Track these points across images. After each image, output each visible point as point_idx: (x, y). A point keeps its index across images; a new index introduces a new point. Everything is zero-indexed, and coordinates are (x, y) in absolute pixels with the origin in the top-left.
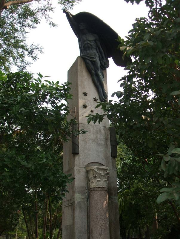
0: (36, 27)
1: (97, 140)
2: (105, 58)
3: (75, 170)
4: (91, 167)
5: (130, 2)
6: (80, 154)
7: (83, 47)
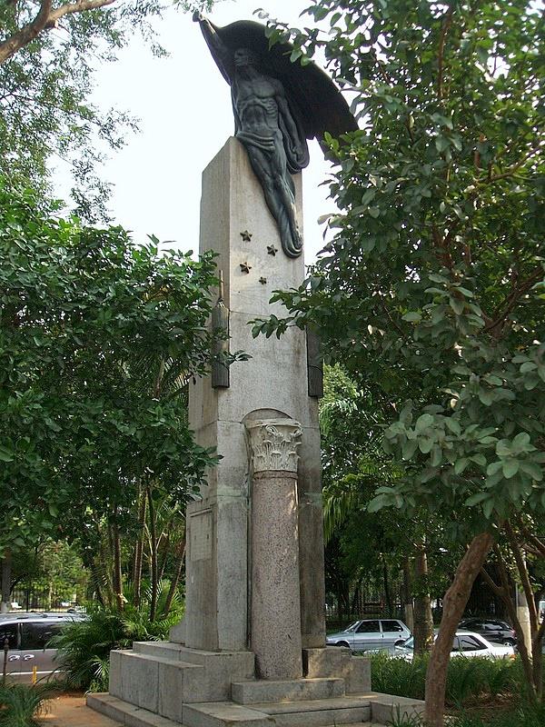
0: (116, 59)
2: (298, 143)
3: (219, 427)
4: (257, 421)
7: (245, 113)
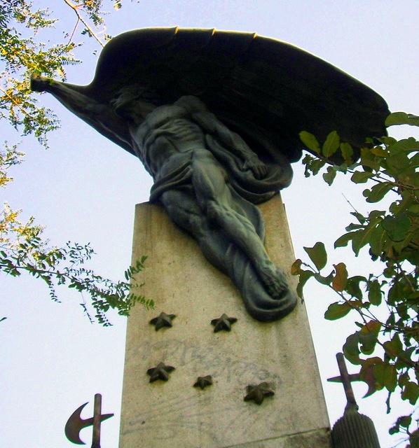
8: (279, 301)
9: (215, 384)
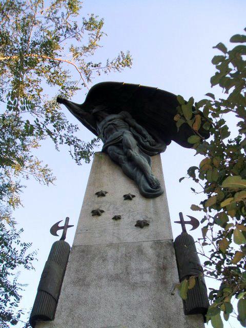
1: (128, 274)
5: (219, 71)
6: (57, 320)
8: (155, 190)
9: (122, 219)
